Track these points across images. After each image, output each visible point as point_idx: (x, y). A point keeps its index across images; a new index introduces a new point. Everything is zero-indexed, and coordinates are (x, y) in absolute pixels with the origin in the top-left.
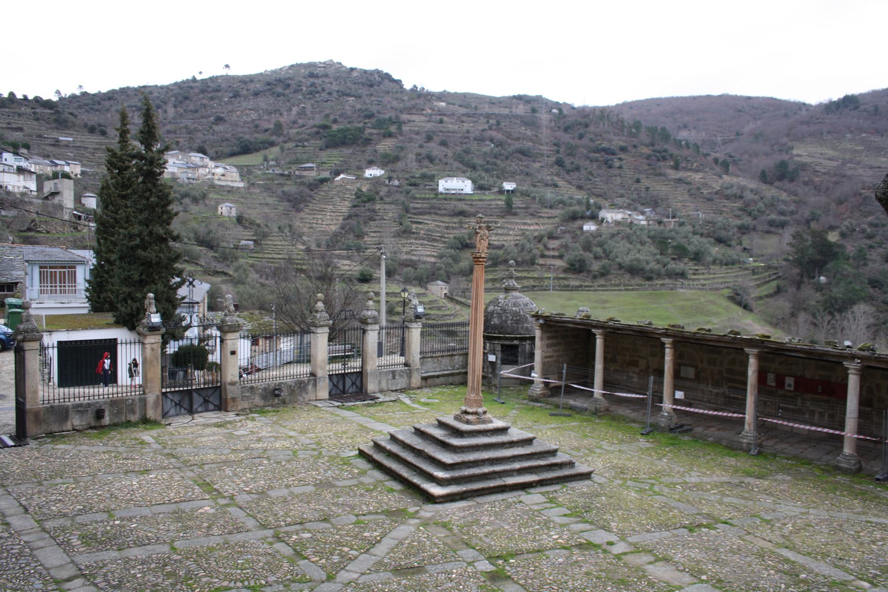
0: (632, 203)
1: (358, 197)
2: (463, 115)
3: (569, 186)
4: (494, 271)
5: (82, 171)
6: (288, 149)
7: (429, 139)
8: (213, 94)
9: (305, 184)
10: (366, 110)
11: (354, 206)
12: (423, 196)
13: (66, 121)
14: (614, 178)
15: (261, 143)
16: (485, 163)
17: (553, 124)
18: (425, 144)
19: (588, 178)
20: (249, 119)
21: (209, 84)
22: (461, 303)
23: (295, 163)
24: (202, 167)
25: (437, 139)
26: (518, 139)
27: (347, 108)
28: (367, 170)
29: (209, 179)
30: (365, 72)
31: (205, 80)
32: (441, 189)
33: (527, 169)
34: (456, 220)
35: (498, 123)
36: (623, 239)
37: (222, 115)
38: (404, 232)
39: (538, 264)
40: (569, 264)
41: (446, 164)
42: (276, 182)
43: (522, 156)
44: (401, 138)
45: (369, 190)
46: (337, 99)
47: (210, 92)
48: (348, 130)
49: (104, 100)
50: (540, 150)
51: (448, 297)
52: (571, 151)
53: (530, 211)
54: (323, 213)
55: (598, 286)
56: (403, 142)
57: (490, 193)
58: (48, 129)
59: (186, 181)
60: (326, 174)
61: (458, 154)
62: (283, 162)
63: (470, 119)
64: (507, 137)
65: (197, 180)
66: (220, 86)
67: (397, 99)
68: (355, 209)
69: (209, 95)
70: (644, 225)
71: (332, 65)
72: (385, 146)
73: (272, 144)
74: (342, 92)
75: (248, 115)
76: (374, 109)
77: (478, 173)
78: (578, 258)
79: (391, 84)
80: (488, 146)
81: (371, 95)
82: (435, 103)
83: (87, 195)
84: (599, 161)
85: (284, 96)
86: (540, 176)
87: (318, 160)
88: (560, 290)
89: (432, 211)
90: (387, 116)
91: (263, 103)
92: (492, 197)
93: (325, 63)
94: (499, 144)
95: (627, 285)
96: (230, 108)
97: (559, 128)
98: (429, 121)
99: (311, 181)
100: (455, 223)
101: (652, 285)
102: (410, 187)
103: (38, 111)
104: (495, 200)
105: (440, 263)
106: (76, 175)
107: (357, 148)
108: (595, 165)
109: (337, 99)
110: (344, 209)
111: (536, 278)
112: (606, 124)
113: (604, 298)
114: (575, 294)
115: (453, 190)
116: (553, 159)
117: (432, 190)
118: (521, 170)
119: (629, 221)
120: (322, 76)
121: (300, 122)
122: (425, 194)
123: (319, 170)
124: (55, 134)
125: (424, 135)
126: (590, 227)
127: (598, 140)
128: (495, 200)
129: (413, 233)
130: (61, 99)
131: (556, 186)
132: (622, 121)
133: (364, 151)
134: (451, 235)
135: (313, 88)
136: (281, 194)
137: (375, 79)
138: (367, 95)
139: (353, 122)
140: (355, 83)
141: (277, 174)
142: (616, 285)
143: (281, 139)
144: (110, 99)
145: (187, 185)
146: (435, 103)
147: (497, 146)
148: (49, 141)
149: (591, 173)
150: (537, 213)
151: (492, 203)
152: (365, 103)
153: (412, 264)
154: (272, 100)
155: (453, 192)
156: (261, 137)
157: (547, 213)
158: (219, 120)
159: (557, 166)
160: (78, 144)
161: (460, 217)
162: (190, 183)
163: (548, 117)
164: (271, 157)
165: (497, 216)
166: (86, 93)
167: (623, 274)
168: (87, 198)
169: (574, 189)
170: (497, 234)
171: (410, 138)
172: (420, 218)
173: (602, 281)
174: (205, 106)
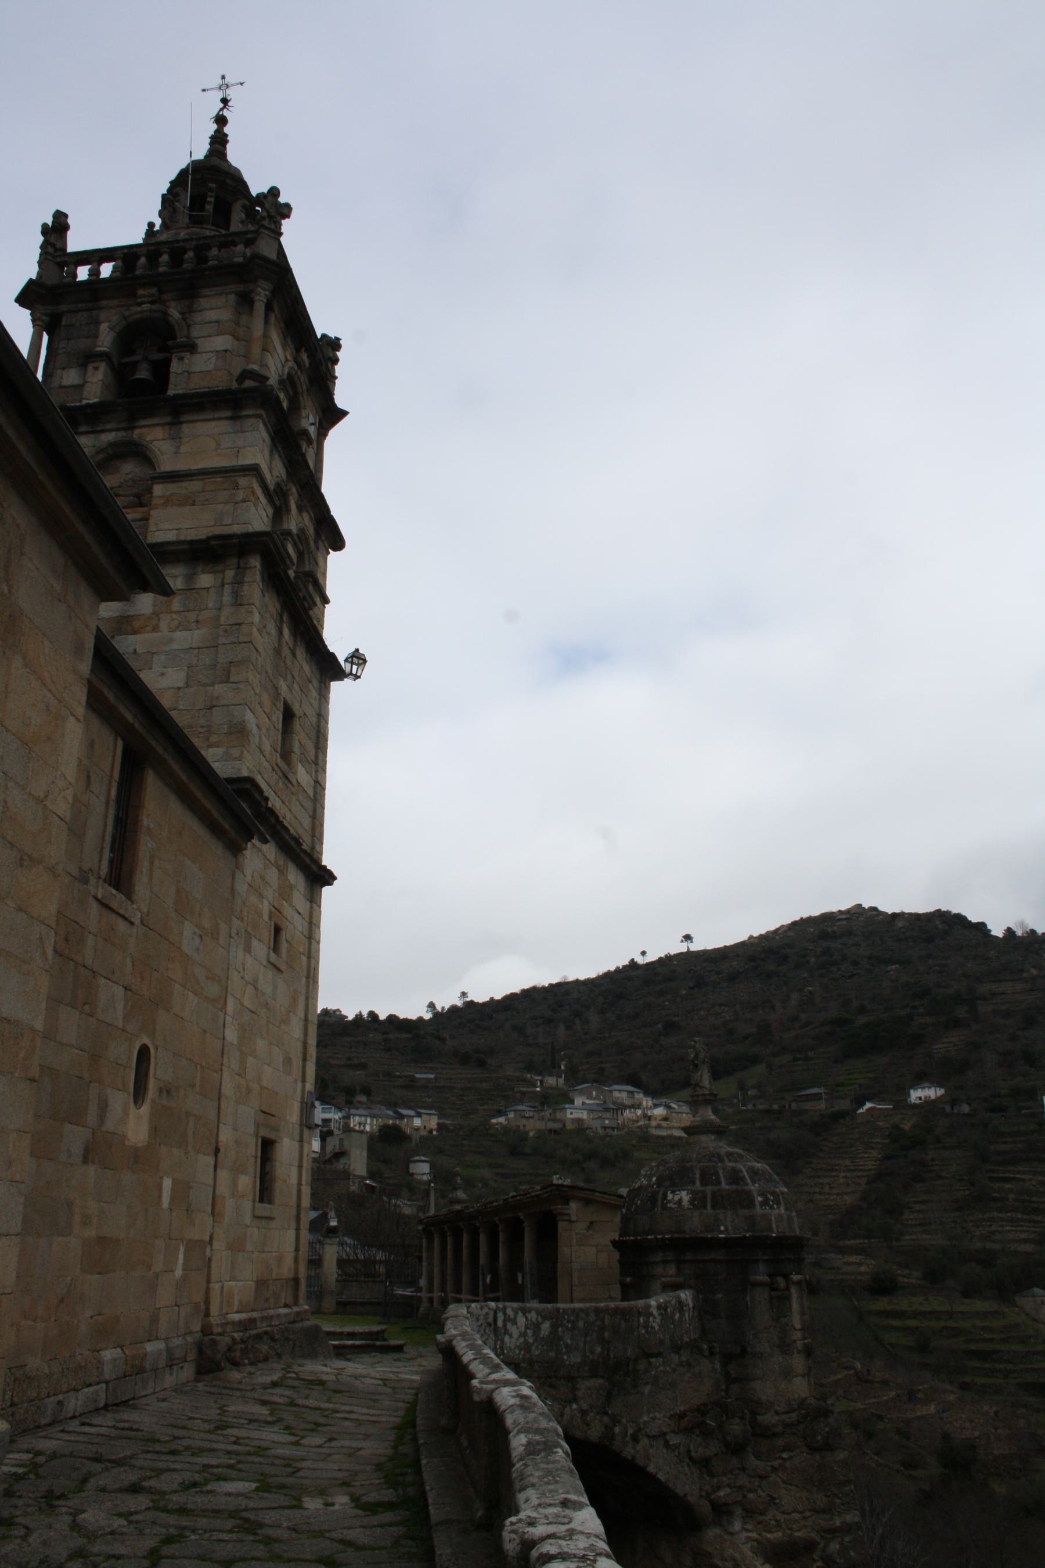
5: (438, 1124)
28: (912, 1092)
29: (639, 1127)
30: (917, 917)
37: (676, 1019)
42: (758, 1125)
54: (834, 1174)
59: (601, 1131)
60: (844, 1105)
65: (618, 1128)
73: (755, 1060)
83: (417, 1158)
103: (391, 1036)
106: (431, 1131)
129: (995, 1199)
130: (437, 1016)
162: (607, 1135)
166: (472, 1002)
168: (417, 1164)
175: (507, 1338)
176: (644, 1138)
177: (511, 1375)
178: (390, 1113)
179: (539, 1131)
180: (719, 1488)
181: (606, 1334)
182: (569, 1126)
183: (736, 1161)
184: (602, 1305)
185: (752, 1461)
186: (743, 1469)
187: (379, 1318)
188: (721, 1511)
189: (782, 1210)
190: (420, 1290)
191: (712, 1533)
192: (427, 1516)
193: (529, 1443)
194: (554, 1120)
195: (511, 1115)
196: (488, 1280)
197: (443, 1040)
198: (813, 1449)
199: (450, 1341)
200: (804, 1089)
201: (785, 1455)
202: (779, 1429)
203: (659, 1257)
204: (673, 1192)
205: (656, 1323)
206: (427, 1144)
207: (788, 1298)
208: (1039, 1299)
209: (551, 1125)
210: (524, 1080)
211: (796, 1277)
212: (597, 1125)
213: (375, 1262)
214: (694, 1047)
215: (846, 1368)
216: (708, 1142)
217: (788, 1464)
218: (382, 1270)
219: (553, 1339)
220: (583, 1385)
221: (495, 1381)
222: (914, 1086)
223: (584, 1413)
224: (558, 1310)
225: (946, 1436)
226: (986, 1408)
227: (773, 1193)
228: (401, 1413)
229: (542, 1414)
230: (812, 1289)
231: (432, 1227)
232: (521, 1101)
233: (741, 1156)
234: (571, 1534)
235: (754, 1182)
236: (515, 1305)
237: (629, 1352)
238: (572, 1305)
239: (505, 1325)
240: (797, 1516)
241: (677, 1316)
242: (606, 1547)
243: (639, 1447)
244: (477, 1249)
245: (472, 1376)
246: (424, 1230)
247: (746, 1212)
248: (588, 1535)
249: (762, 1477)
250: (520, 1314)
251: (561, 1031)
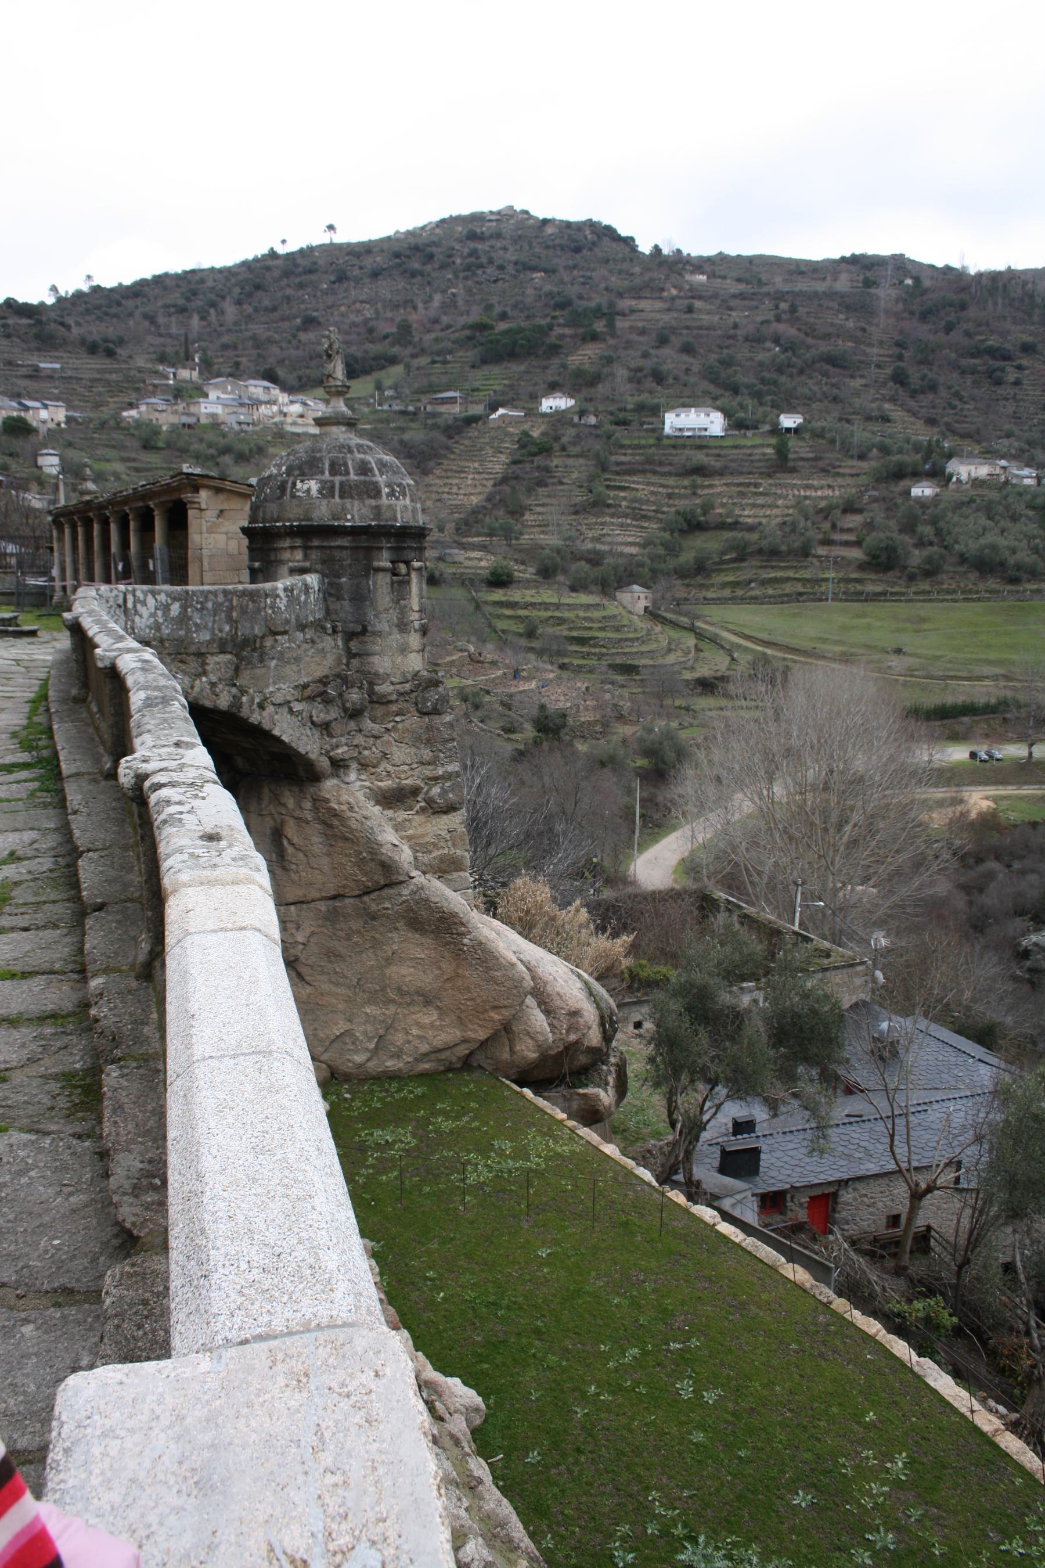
0: (1027, 447)
1: (523, 447)
2: (734, 296)
3: (912, 419)
4: (738, 569)
5: (67, 417)
6: (418, 369)
7: (663, 341)
8: (303, 278)
9: (439, 427)
10: (559, 293)
11: (514, 462)
12: (636, 442)
13: (52, 337)
14: (1003, 402)
15: (374, 359)
16: (756, 382)
17: (900, 306)
18: (653, 352)
19: (950, 404)
20: (359, 319)
21: (299, 261)
22: (671, 622)
23: (428, 392)
24: (268, 403)
25: (676, 341)
26: (827, 336)
27: (530, 291)
29: (275, 424)
30: (568, 225)
31: (292, 254)
32: (667, 430)
33: (835, 391)
34: (686, 482)
35: (793, 309)
36: (978, 510)
37: (315, 314)
38: (595, 504)
39: (815, 556)
40: (868, 555)
41: (685, 385)
42: (392, 425)
43: (829, 367)
44: (611, 342)
45: (543, 434)
46: (515, 277)
47: (300, 275)
48: (521, 330)
49: (127, 297)
50: (866, 354)
51: (651, 613)
52: (926, 355)
53: (821, 464)
55: (915, 593)
56: (615, 348)
57: (754, 435)
58: (24, 350)
59: (236, 427)
60: (478, 409)
61: (710, 367)
62: (407, 391)
63: (747, 303)
64: (807, 334)
65: (254, 424)
66: (315, 263)
67: (620, 272)
68: (515, 467)
69: (297, 281)
70: (1029, 486)
71: (512, 216)
72: (583, 357)
73: (393, 361)
74: (523, 264)
75: (358, 311)
76: (572, 291)
77: (739, 398)
78: (883, 545)
79: (614, 245)
80: (769, 350)
81: (575, 267)
82: (688, 277)
84: (979, 372)
85: (423, 276)
86: (857, 402)
87: (467, 386)
88: (846, 600)
89: (648, 467)
90: (592, 304)
91: (386, 289)
92: (758, 441)
93: (499, 213)
94: (790, 347)
95: (970, 592)
96: (330, 300)
97: (912, 313)
98: (669, 310)
99: (450, 422)
100: (685, 488)
101: (1018, 592)
102: (614, 427)
103: (10, 321)
104: (763, 446)
105: (643, 555)
106: (59, 424)
107: (534, 363)
108: (969, 379)
109: (515, 277)
110: (498, 468)
111: (808, 580)
112: (1000, 301)
113: (922, 613)
114: (870, 607)
115: (689, 429)
116: (889, 371)
117: (653, 430)
118: (824, 393)
119: (1003, 478)
120: (491, 237)
121: (445, 319)
122: (639, 438)
123: (466, 401)
124: (34, 360)
125: (654, 336)
126: (923, 490)
127: (981, 334)
128: (763, 446)
129: (609, 506)
130: (60, 300)
131: (886, 419)
132: (1031, 296)
133: (546, 368)
134: (670, 510)
135: (472, 260)
136: (398, 446)
137: (585, 237)
138: (566, 268)
139: (534, 316)
140: (547, 247)
141: (395, 412)
142: (949, 592)
143: (409, 350)
144: (136, 295)
145: (238, 433)
146: (688, 277)
147: (785, 350)
148: (24, 371)
149: (957, 395)
150: (834, 467)
151: (756, 451)
152: (562, 282)
153: (595, 559)
154: (401, 285)
155: (689, 434)
156: (375, 349)
157: (852, 467)
158: (310, 322)
159: (891, 384)
160: (69, 373)
161: (695, 477)
162: (242, 431)
163: (894, 293)
164: (388, 382)
165: (761, 473)
166: (99, 287)
167: (965, 573)
169: (920, 424)
170: (754, 506)
171: (628, 342)
172: (625, 481)
173: (925, 586)
174: (288, 299)
175: (137, 619)
176: (280, 435)
177: (136, 645)
178: (14, 404)
179: (173, 425)
180: (337, 746)
181: (234, 614)
182: (204, 421)
183: (365, 453)
184: (230, 587)
185: (368, 724)
186: (360, 731)
187: (12, 608)
188: (338, 765)
189: (408, 501)
190: (53, 579)
191: (330, 783)
192: (60, 773)
193: (147, 698)
194: (188, 414)
195: (143, 408)
196: (120, 567)
197: (68, 328)
198: (423, 714)
199: (77, 618)
200: (441, 391)
201: (398, 719)
202: (394, 697)
203: (287, 543)
204: (302, 481)
205: (282, 604)
206: (55, 437)
207: (408, 583)
208: (636, 595)
209: (185, 419)
210: (156, 372)
211: (416, 564)
212: (231, 420)
213: (5, 554)
214: (328, 337)
215: (461, 651)
216: (339, 433)
217: (400, 726)
218: (13, 561)
219: (183, 619)
220: (212, 660)
221: (119, 649)
222: (546, 395)
223: (213, 685)
224: (187, 592)
225: (543, 707)
226: (579, 684)
227: (399, 485)
228: (36, 689)
229: (161, 675)
230: (433, 581)
231: (61, 518)
232: (153, 394)
233: (370, 448)
234: (182, 766)
235: (382, 474)
236: (145, 587)
237: (257, 631)
238: (201, 588)
239: (135, 606)
240: (406, 768)
241: (303, 598)
242: (216, 778)
243: (265, 713)
244: (109, 539)
245: (97, 646)
246: (54, 521)
247: (373, 502)
248: (198, 767)
249: (376, 737)
250: (150, 596)
251: (195, 321)
